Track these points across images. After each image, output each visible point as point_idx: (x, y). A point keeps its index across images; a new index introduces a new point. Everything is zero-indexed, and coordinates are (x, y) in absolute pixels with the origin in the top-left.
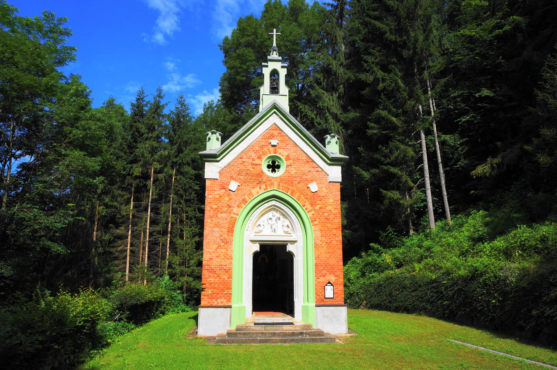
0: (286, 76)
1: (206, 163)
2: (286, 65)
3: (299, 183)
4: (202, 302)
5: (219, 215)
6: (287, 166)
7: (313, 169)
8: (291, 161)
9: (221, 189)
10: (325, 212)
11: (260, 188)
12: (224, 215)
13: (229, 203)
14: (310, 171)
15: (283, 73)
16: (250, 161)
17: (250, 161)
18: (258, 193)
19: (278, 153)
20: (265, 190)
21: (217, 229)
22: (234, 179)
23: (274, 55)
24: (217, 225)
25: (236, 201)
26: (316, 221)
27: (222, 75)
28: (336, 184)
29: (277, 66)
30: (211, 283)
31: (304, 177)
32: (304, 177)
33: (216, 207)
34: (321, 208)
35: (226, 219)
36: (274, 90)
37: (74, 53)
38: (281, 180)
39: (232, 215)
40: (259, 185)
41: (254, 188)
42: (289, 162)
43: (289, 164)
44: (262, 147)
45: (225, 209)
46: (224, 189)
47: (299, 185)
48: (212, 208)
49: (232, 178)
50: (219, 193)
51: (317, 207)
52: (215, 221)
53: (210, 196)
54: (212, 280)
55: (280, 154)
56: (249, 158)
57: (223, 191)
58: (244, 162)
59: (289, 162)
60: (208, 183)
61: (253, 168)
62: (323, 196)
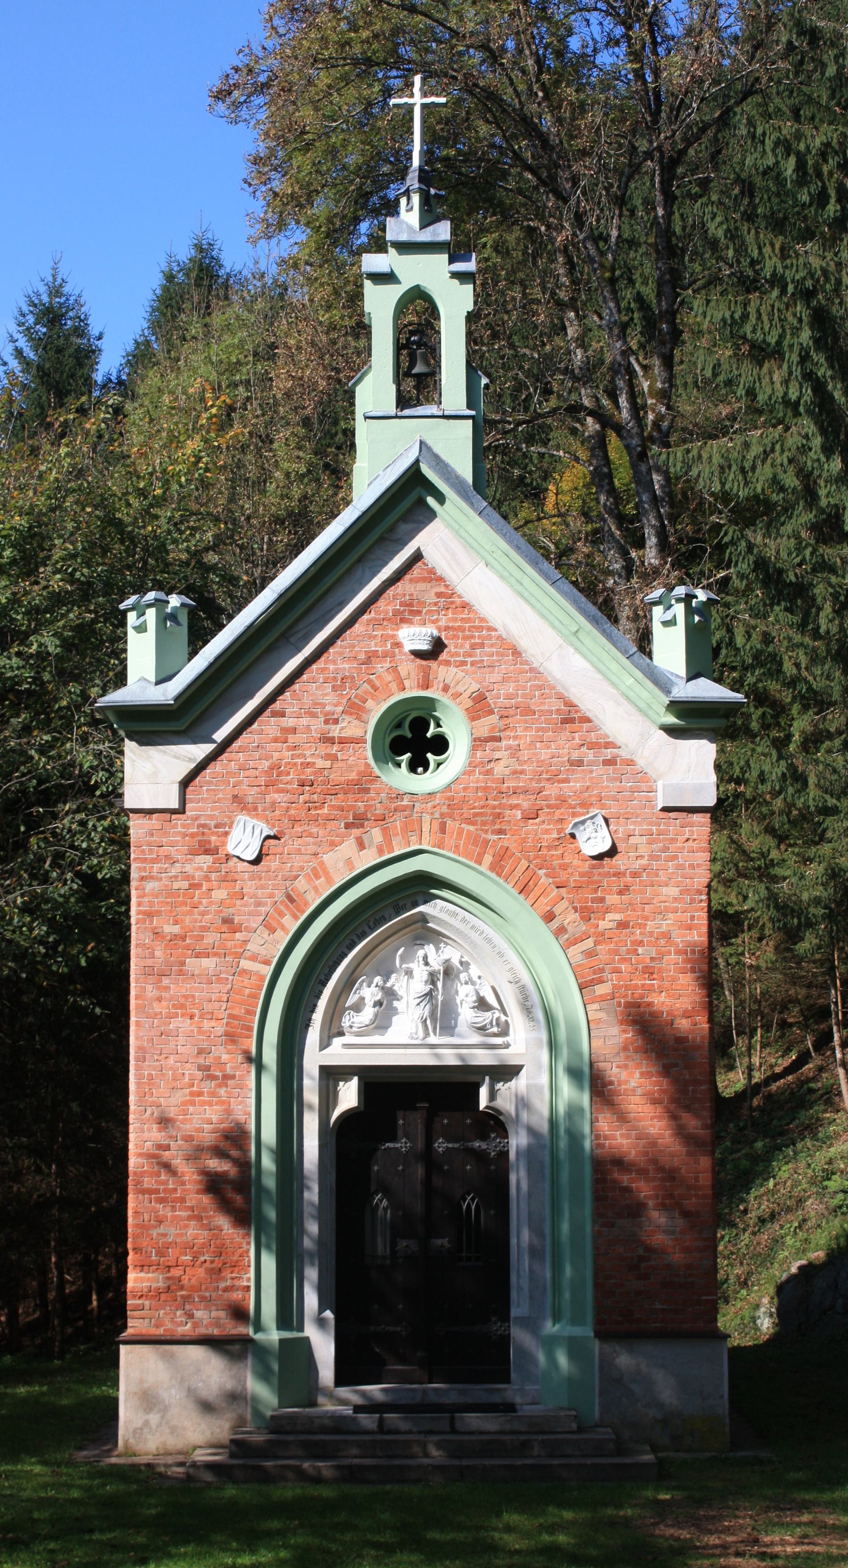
0: (471, 318)
1: (177, 807)
2: (470, 266)
3: (527, 818)
4: (130, 1323)
5: (191, 963)
6: (478, 743)
7: (590, 755)
8: (493, 719)
9: (194, 853)
10: (641, 943)
11: (361, 845)
12: (208, 963)
13: (228, 912)
14: (580, 763)
15: (455, 303)
16: (317, 725)
17: (317, 725)
18: (349, 863)
19: (438, 685)
20: (381, 852)
21: (181, 1024)
22: (250, 809)
23: (407, 221)
24: (181, 1007)
25: (258, 904)
26: (601, 981)
27: (130, 347)
28: (697, 818)
29: (433, 273)
30: (167, 1246)
31: (552, 790)
32: (552, 790)
33: (176, 929)
34: (623, 925)
35: (219, 980)
36: (416, 384)
37: (671, 719)
38: (451, 802)
39: (245, 964)
40: (356, 832)
41: (333, 844)
42: (485, 725)
43: (484, 732)
44: (368, 661)
45: (211, 938)
46: (207, 852)
47: (532, 825)
48: (157, 934)
49: (240, 802)
50: (188, 868)
51: (607, 923)
52: (176, 988)
53: (150, 886)
54: (172, 1231)
55: (446, 689)
56: (314, 715)
57: (205, 861)
58: (294, 730)
59: (485, 725)
60: (137, 828)
61: (328, 757)
62: (635, 875)
